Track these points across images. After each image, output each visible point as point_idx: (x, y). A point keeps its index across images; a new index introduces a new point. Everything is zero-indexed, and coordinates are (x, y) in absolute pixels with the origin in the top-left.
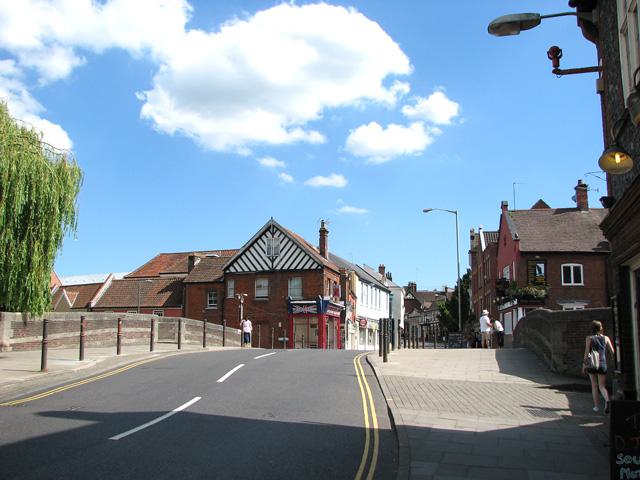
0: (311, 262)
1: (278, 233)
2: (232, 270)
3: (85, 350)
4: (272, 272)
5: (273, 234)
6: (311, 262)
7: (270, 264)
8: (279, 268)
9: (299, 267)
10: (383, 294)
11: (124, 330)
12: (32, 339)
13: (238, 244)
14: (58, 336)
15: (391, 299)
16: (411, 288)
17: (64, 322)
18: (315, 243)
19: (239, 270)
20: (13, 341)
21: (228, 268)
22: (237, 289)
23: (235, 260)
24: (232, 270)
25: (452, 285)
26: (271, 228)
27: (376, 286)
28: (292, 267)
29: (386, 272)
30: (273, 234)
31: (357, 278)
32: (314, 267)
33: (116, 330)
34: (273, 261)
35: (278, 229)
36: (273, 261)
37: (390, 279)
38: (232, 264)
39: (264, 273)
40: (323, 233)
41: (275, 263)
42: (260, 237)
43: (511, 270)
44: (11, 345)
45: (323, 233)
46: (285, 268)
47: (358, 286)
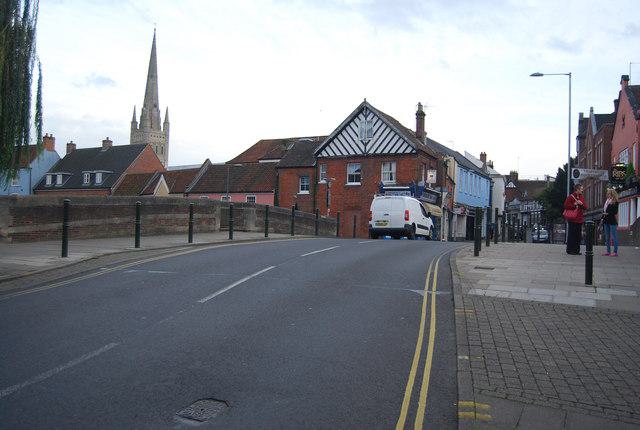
0: (405, 145)
1: (371, 115)
2: (324, 154)
3: (70, 243)
4: (365, 156)
5: (366, 117)
6: (405, 145)
7: (363, 148)
8: (371, 152)
9: (393, 151)
10: (484, 181)
11: (195, 215)
12: (127, 219)
13: (327, 130)
14: (79, 223)
15: (491, 187)
16: (513, 176)
17: (90, 207)
18: (411, 124)
19: (332, 154)
20: (12, 231)
21: (319, 152)
22: (329, 174)
23: (328, 144)
24: (324, 154)
25: (554, 174)
26: (364, 109)
27: (476, 172)
28: (386, 151)
29: (488, 160)
30: (366, 117)
31: (456, 164)
32: (408, 151)
33: (187, 216)
34: (366, 145)
35: (371, 111)
36: (366, 145)
37: (492, 167)
38: (324, 148)
39: (356, 156)
40: (420, 116)
41: (368, 147)
42: (352, 120)
43: (630, 154)
44: (10, 235)
45: (420, 116)
46: (378, 152)
47: (44, 135)
